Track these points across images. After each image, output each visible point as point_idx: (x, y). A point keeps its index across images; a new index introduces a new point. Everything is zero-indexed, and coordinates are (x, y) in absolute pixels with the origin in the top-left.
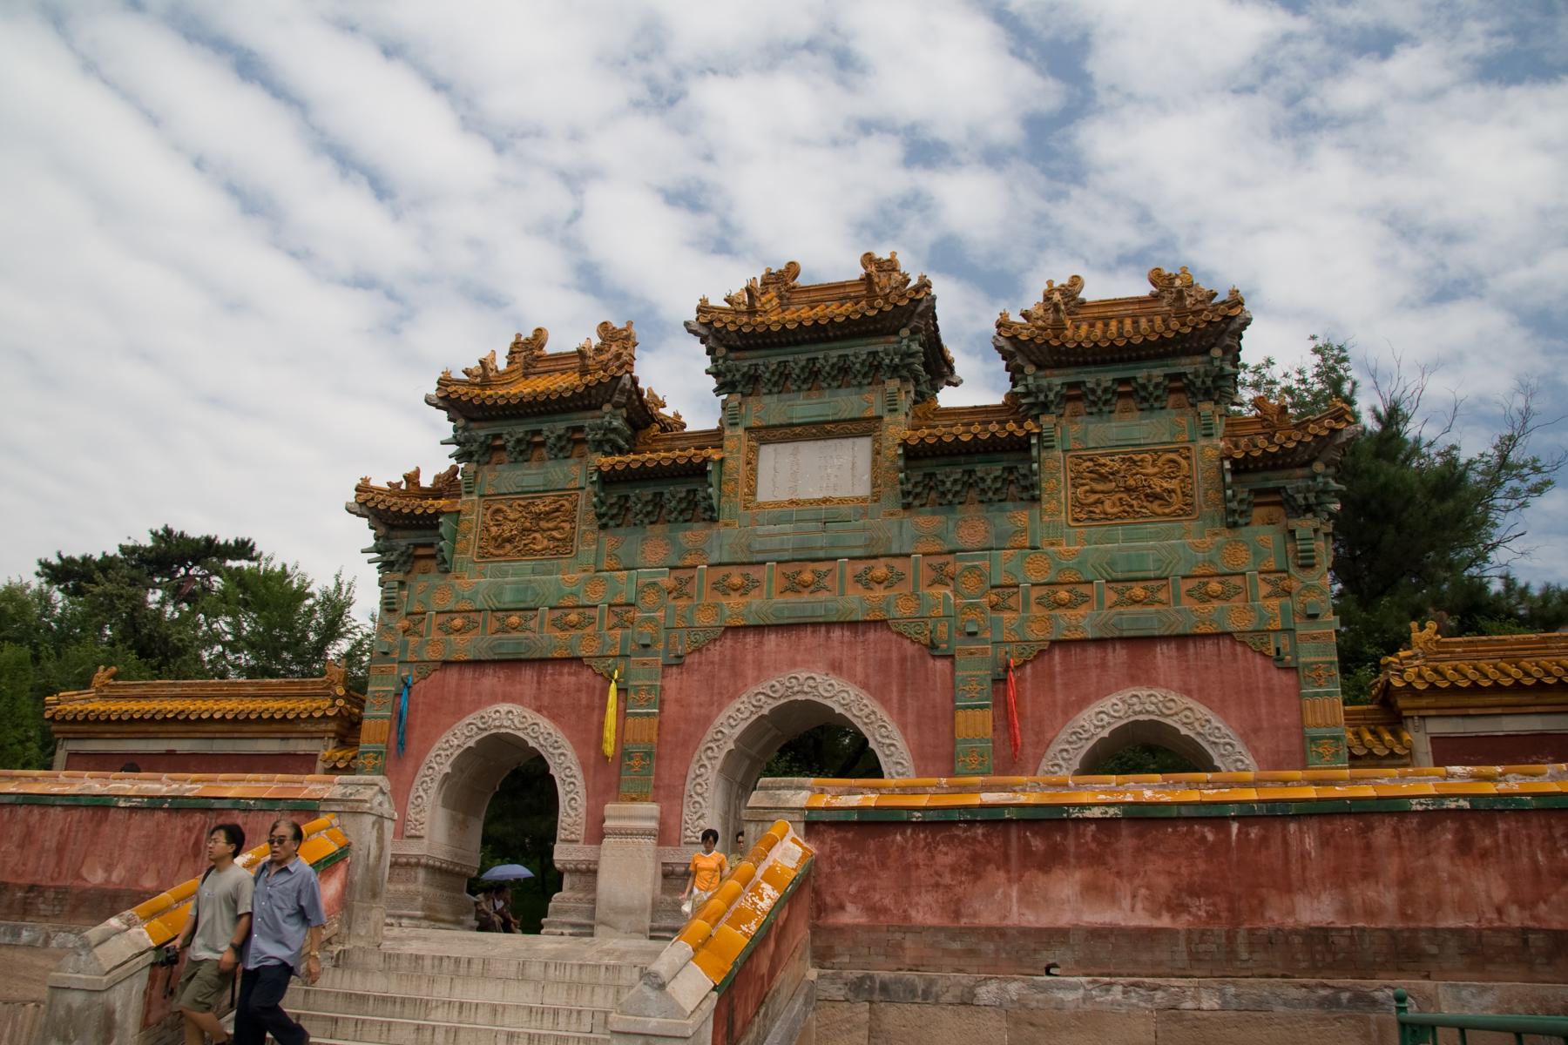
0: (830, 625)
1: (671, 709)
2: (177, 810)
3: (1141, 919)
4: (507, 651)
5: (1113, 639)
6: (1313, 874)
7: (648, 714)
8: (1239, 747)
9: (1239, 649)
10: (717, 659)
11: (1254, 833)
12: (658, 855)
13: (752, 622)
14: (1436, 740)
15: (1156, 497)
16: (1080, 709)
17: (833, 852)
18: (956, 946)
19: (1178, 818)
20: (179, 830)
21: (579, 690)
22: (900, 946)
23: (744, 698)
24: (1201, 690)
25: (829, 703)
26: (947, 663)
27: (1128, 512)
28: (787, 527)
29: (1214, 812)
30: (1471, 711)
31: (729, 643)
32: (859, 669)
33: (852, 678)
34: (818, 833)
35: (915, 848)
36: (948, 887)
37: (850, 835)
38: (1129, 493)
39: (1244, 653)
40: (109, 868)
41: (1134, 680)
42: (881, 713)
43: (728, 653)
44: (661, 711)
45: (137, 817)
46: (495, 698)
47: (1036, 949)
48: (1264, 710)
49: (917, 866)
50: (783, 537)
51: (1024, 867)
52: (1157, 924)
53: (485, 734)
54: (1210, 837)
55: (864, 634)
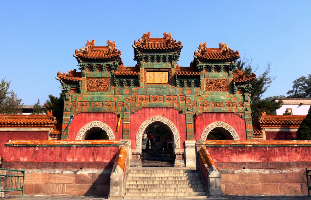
0: (162, 107)
1: (132, 122)
2: (88, 147)
3: (256, 161)
4: (96, 110)
5: (213, 112)
6: (278, 155)
7: (128, 123)
8: (235, 132)
9: (235, 115)
10: (141, 113)
11: (270, 149)
12: (131, 151)
13: (148, 106)
14: (266, 132)
15: (221, 88)
16: (208, 125)
17: (211, 151)
18: (230, 165)
19: (260, 147)
20: (88, 151)
21: (113, 118)
22: (222, 165)
23: (147, 120)
24: (228, 122)
25: (163, 122)
26: (185, 115)
27: (216, 90)
28: (154, 89)
29: (265, 146)
30: (272, 127)
31: (143, 110)
32: (168, 116)
33: (167, 117)
34: (208, 148)
35: (223, 151)
36: (228, 156)
37: (213, 149)
38: (215, 86)
39: (236, 116)
40: (73, 158)
41: (217, 120)
42: (173, 124)
43: (143, 112)
44: (130, 123)
45: (78, 149)
46: (94, 120)
47: (243, 166)
48: (239, 126)
49: (223, 153)
50: (152, 90)
51: (239, 154)
52: (258, 162)
53: (92, 127)
54: (264, 149)
55: (169, 109)
